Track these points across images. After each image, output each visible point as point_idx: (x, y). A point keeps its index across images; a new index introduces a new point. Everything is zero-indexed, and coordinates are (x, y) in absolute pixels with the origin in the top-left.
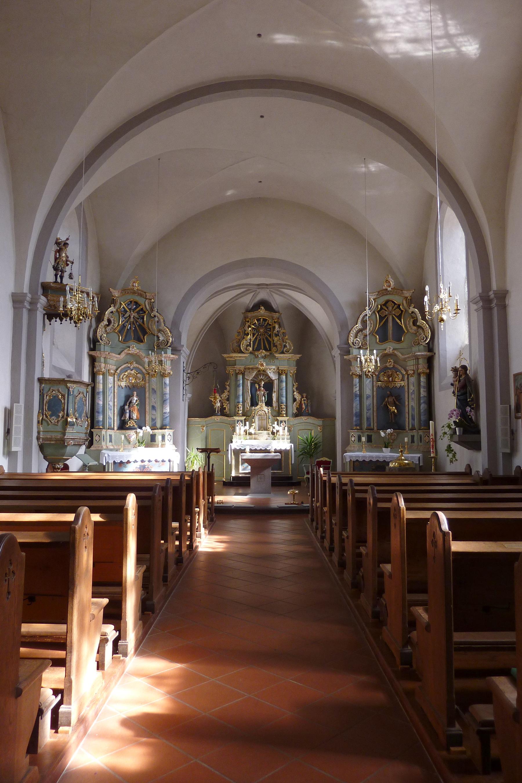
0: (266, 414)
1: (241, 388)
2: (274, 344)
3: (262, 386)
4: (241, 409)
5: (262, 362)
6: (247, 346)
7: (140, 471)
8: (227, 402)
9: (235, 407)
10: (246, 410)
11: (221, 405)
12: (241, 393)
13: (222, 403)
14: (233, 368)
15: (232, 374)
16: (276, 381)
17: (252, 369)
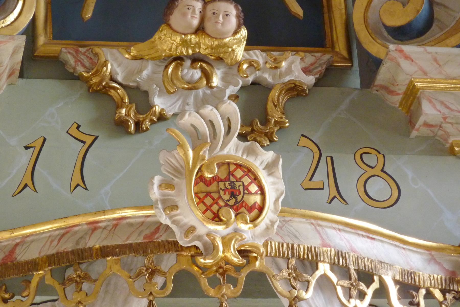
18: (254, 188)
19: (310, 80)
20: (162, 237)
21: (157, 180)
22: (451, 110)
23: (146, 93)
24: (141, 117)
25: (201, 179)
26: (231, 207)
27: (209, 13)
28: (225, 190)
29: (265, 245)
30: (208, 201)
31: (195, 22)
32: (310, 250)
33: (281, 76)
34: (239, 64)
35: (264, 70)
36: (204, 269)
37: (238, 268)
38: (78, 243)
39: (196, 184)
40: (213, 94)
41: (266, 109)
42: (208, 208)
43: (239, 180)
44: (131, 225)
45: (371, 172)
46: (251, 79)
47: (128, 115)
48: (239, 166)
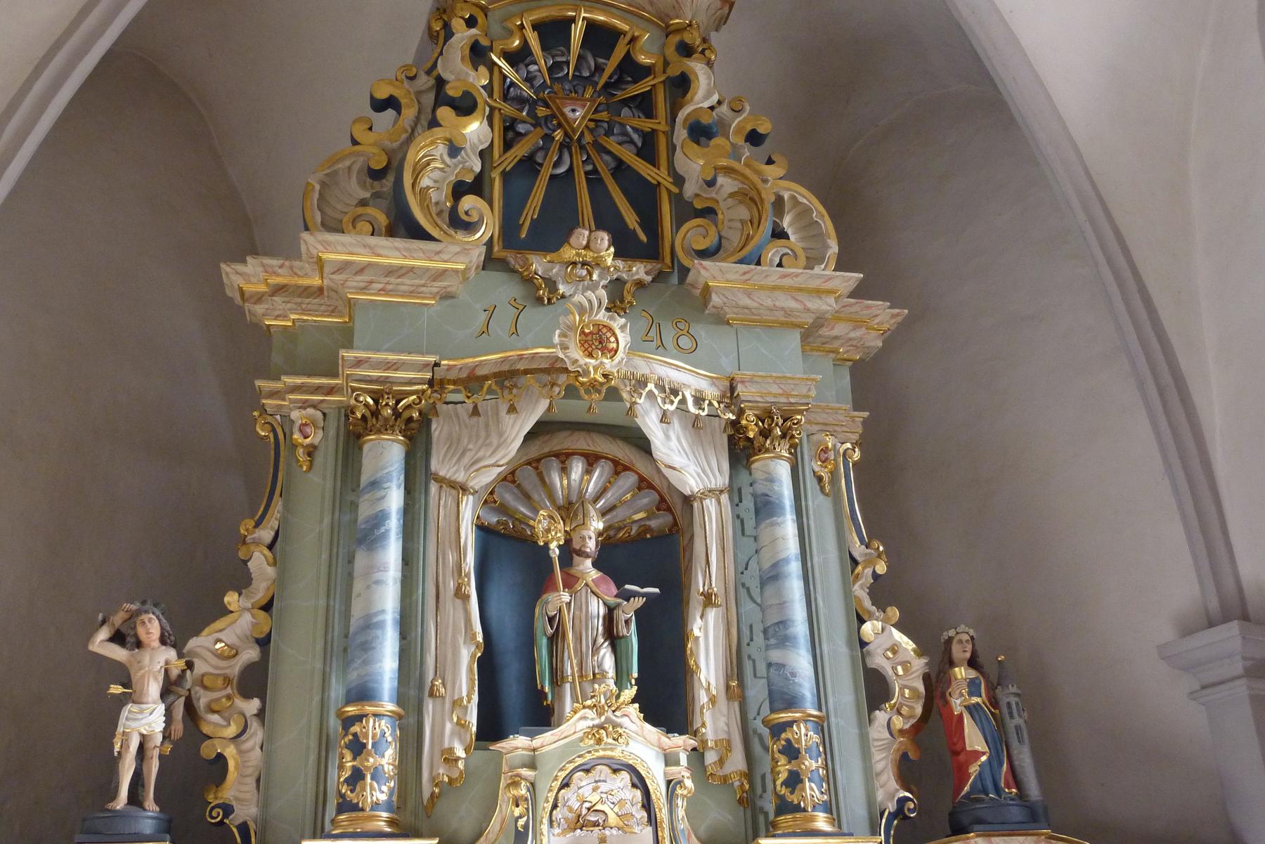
0: (647, 804)
1: (392, 553)
2: (678, 201)
3: (591, 545)
4: (387, 759)
5: (602, 316)
6: (459, 190)
7: (1011, 807)
8: (240, 703)
9: (325, 746)
10: (435, 781)
11: (178, 728)
12: (388, 599)
13: (190, 708)
14: (317, 389)
15: (311, 451)
16: (710, 505)
17: (507, 378)
18: (612, 339)
19: (649, 278)
20: (558, 365)
21: (558, 332)
23: (555, 282)
25: (582, 332)
26: (599, 349)
27: (592, 238)
29: (618, 372)
30: (586, 346)
31: (584, 243)
33: (632, 275)
34: (609, 268)
35: (623, 272)
36: (582, 384)
37: (602, 384)
38: (511, 365)
43: (604, 334)
44: (541, 357)
45: (681, 333)
46: (615, 277)
47: (544, 294)
48: (605, 326)
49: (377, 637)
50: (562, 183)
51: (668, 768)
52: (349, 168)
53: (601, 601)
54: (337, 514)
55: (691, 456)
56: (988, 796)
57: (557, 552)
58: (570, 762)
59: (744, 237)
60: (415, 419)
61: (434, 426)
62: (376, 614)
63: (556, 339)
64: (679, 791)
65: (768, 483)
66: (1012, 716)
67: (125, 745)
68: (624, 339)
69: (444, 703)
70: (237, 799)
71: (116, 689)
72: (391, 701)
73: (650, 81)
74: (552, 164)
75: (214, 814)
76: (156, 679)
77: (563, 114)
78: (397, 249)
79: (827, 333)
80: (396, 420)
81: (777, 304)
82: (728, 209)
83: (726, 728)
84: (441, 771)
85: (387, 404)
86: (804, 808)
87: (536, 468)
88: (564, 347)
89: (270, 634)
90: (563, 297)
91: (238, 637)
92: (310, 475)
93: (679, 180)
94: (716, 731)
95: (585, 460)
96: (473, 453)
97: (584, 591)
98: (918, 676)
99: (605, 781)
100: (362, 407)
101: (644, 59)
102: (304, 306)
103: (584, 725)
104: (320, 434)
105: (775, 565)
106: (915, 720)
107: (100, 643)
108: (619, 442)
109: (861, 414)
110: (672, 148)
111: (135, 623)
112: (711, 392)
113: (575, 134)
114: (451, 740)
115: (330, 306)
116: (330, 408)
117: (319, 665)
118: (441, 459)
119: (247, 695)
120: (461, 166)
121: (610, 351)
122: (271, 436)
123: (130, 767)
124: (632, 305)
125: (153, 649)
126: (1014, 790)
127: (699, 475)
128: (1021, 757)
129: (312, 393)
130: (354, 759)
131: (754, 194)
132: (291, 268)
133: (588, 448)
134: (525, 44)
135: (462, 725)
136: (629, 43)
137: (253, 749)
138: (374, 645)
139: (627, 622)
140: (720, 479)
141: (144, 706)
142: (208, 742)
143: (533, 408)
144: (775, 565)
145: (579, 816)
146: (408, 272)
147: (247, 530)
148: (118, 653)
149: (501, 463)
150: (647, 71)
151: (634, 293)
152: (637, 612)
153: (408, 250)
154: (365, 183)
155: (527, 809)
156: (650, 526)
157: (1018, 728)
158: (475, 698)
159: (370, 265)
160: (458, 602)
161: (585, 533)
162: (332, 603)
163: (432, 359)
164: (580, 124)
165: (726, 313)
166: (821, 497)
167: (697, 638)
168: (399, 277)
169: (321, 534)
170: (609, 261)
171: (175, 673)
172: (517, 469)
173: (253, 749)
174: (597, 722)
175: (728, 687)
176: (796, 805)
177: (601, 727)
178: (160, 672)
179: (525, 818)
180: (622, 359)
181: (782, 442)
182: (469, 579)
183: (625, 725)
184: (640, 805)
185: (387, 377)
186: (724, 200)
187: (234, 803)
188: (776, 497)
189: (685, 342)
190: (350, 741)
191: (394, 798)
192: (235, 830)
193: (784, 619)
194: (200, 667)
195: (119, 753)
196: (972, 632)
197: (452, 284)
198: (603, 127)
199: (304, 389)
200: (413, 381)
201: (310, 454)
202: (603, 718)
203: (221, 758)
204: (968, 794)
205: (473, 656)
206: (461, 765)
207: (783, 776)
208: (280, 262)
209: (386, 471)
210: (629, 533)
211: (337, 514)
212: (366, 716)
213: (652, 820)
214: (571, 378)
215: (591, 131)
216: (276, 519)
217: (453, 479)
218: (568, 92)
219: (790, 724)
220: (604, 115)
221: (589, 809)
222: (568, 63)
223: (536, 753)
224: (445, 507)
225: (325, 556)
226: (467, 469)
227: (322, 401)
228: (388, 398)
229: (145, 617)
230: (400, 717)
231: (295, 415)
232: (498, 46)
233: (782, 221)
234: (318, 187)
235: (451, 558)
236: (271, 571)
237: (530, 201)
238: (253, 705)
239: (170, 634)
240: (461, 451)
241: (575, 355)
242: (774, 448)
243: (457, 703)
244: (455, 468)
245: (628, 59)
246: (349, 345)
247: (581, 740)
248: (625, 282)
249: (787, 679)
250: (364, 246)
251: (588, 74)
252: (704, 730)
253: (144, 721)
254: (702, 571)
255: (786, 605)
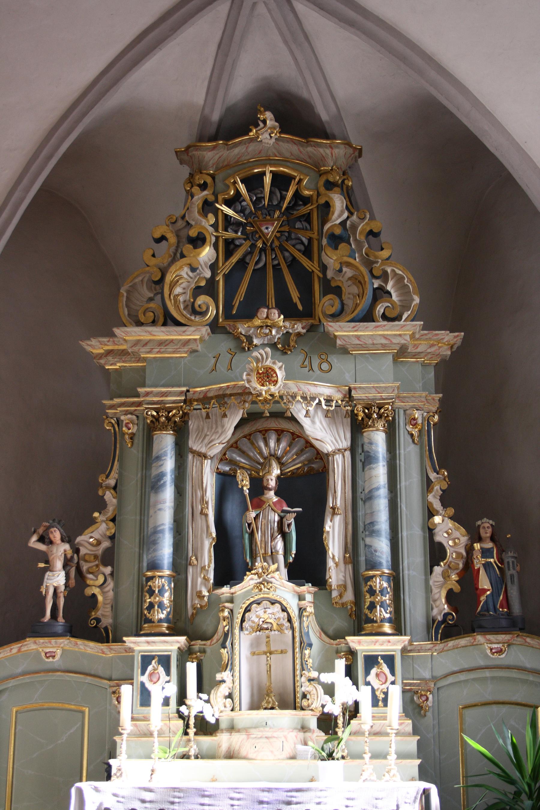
0: (290, 620)
3: (272, 483)
4: (166, 598)
8: (102, 568)
11: (72, 582)
14: (133, 404)
15: (132, 437)
16: (338, 458)
18: (274, 375)
19: (304, 331)
20: (247, 391)
21: (245, 373)
22: (346, 342)
23: (252, 338)
24: (249, 346)
25: (258, 373)
26: (267, 381)
27: (269, 313)
28: (265, 376)
29: (279, 392)
30: (260, 380)
31: (265, 316)
32: (294, 393)
33: (295, 330)
34: (281, 327)
35: (289, 328)
36: (260, 400)
37: (270, 400)
38: (224, 392)
39: (257, 374)
40: (273, 337)
41: (289, 342)
42: (260, 382)
43: (270, 373)
44: (238, 387)
45: (323, 361)
46: (285, 332)
47: (245, 346)
48: (270, 368)
49: (159, 537)
50: (260, 272)
51: (300, 602)
52: (142, 281)
53: (276, 514)
54: (144, 472)
55: (328, 431)
56: (489, 613)
57: (248, 491)
58: (248, 600)
59: (354, 305)
60: (177, 422)
61: (190, 423)
62: (159, 526)
63: (245, 377)
64: (305, 614)
65: (369, 445)
66: (509, 569)
67: (47, 591)
68: (280, 374)
69: (197, 568)
70: (103, 615)
71: (42, 565)
72: (168, 569)
73: (309, 207)
74: (255, 262)
75: (92, 622)
76: (60, 559)
77: (261, 231)
78: (163, 332)
79: (414, 351)
80: (168, 422)
81: (375, 342)
82: (349, 286)
83: (343, 579)
84: (196, 602)
85: (162, 415)
86: (376, 620)
87: (249, 439)
88: (249, 381)
89: (114, 534)
90: (256, 346)
91: (101, 535)
92: (132, 449)
93: (324, 268)
94: (337, 580)
95: (276, 433)
96: (209, 437)
97: (267, 508)
98: (463, 546)
99: (269, 608)
100: (150, 417)
101: (306, 193)
102: (123, 359)
103: (252, 582)
104: (136, 427)
105: (371, 491)
106: (459, 571)
107: (33, 542)
108: (293, 422)
109: (438, 395)
110: (320, 248)
111: (48, 532)
112: (338, 396)
113: (268, 242)
114: (201, 587)
115: (136, 358)
116: (140, 413)
117: (137, 550)
118: (194, 440)
119: (106, 565)
120: (198, 277)
121: (273, 382)
122: (112, 429)
123: (50, 602)
124: (295, 347)
125: (58, 544)
126: (505, 610)
127: (332, 442)
128: (512, 591)
129: (129, 407)
130: (150, 598)
131: (360, 278)
132: (114, 341)
133: (276, 426)
134: (238, 193)
135: (206, 579)
136: (297, 184)
137: (109, 591)
138: (158, 541)
139: (289, 525)
140: (346, 443)
141: (54, 573)
142: (89, 588)
143: (237, 414)
144: (371, 491)
145: (258, 625)
146: (170, 343)
147: (102, 480)
148: (42, 547)
149: (224, 442)
150: (306, 200)
151: (296, 341)
152: (295, 519)
153: (167, 331)
154: (151, 286)
155: (229, 623)
156: (313, 467)
157: (512, 576)
158: (212, 565)
159: (150, 341)
160: (203, 517)
161: (269, 477)
162: (143, 518)
163: (184, 389)
164: (270, 237)
165: (348, 348)
166: (412, 446)
167: (328, 532)
168: (166, 346)
169: (137, 481)
170: (281, 324)
171: (69, 556)
172: (238, 441)
173: (109, 591)
174: (259, 581)
175: (345, 557)
176: (122, 638)
177: (261, 583)
178: (61, 555)
179: (228, 627)
180: (281, 385)
181: (379, 421)
182: (208, 505)
183: (273, 582)
184: (286, 620)
185: (162, 400)
186: (347, 281)
187: (101, 617)
188: (373, 453)
189: (325, 366)
190: (148, 589)
191: (171, 616)
192: (102, 630)
193: (373, 521)
194: (83, 551)
195: (45, 595)
196: (491, 522)
197: (193, 346)
198: (285, 235)
199: (126, 404)
200: (176, 401)
201: (131, 438)
202: (261, 579)
203: (94, 596)
204: (480, 611)
205: (211, 544)
206: (206, 599)
207: (367, 604)
208: (108, 339)
209: (163, 451)
210: (303, 471)
211: (144, 472)
212: (155, 577)
213: (292, 628)
214: (254, 397)
215: (278, 238)
216: (117, 473)
217: (200, 451)
218: (265, 216)
219: (374, 576)
220: (286, 228)
221: (263, 622)
222: (264, 198)
223: (234, 595)
224: (196, 466)
225: (139, 494)
226: (206, 446)
227: (136, 410)
228: (163, 412)
229: (52, 530)
230: (174, 577)
231: (122, 418)
232: (220, 198)
233: (386, 285)
234: (125, 294)
235: (199, 494)
236: (115, 501)
237: (239, 290)
238: (108, 570)
239: (65, 537)
240: (204, 436)
241: (255, 385)
242: (374, 425)
243: (203, 568)
244: (201, 445)
245: (297, 195)
246: (144, 385)
247: (252, 589)
248: (291, 334)
249: (372, 553)
250: (146, 332)
251: (277, 203)
252: (330, 580)
253: (55, 580)
254: (332, 496)
255: (374, 513)
